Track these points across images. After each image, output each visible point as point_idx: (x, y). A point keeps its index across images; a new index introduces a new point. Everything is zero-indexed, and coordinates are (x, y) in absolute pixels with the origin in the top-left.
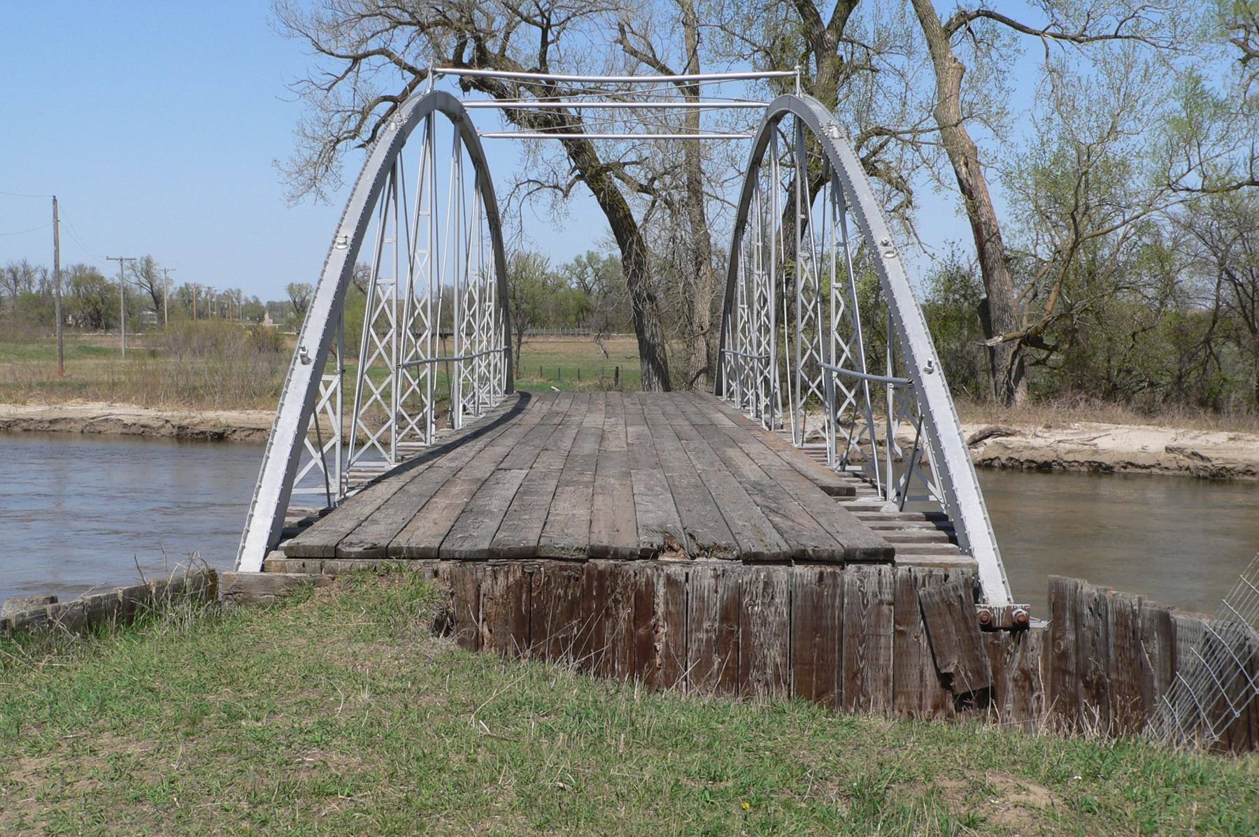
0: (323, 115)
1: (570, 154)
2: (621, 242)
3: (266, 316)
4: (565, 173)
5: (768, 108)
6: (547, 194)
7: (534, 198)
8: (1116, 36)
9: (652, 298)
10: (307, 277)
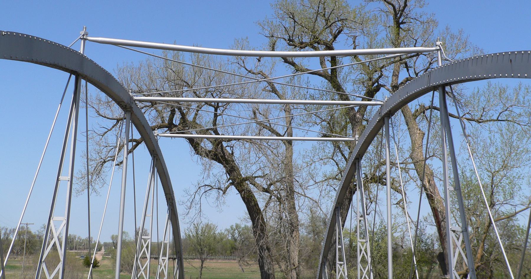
0: (97, 148)
1: (227, 171)
2: (253, 219)
3: (103, 248)
4: (224, 182)
5: (382, 105)
6: (214, 192)
7: (207, 194)
8: (498, 120)
9: (268, 249)
10: (116, 234)
